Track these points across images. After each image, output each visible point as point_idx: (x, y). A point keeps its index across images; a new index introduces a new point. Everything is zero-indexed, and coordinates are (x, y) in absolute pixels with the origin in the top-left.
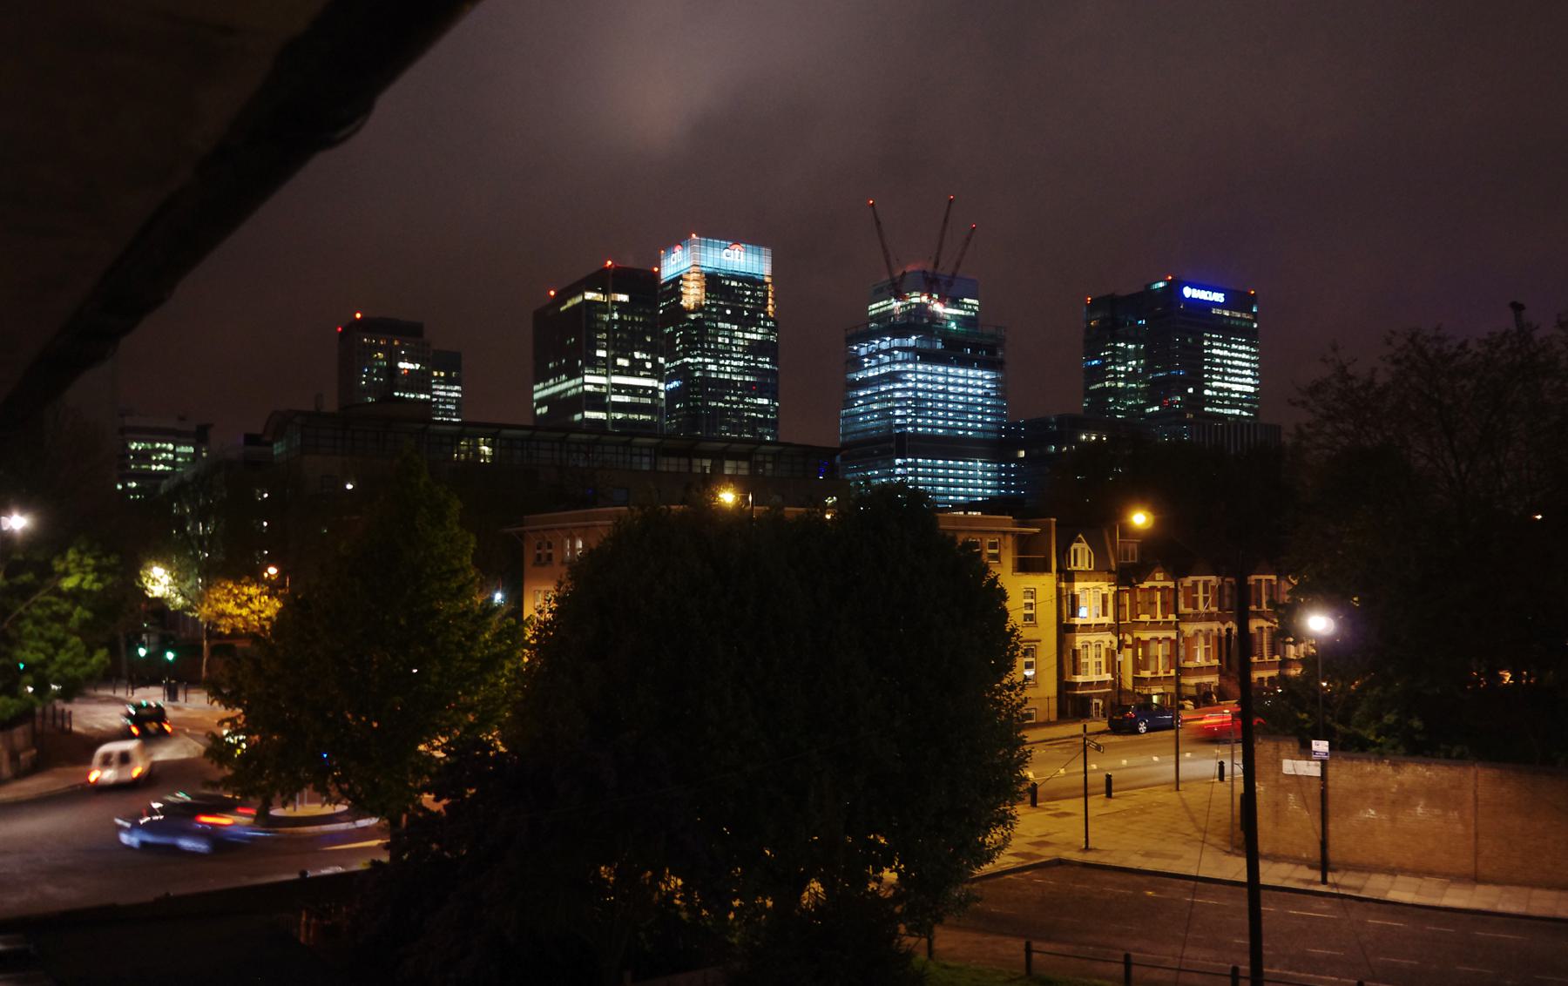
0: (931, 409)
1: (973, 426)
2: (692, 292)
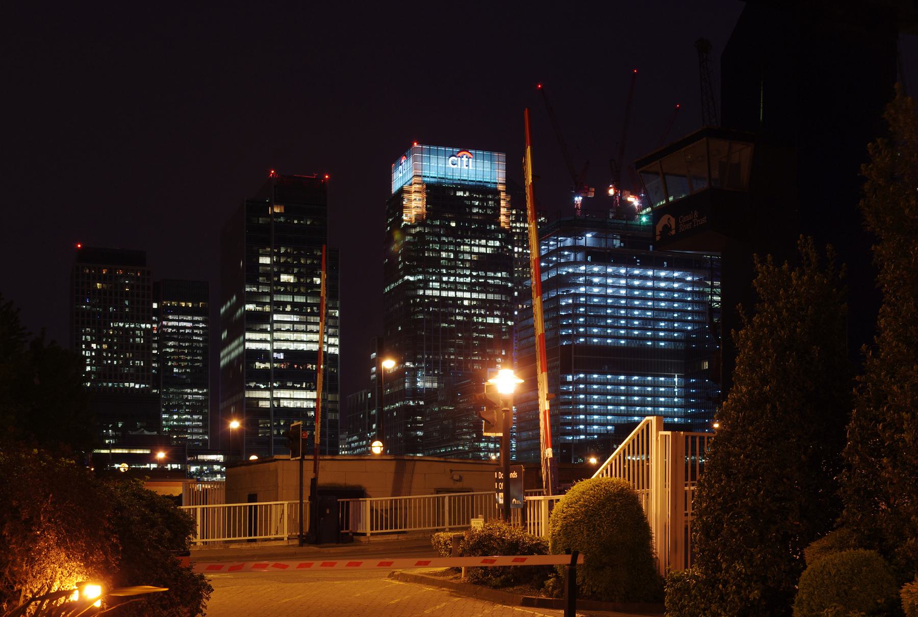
0: (611, 317)
1: (662, 337)
2: (414, 204)
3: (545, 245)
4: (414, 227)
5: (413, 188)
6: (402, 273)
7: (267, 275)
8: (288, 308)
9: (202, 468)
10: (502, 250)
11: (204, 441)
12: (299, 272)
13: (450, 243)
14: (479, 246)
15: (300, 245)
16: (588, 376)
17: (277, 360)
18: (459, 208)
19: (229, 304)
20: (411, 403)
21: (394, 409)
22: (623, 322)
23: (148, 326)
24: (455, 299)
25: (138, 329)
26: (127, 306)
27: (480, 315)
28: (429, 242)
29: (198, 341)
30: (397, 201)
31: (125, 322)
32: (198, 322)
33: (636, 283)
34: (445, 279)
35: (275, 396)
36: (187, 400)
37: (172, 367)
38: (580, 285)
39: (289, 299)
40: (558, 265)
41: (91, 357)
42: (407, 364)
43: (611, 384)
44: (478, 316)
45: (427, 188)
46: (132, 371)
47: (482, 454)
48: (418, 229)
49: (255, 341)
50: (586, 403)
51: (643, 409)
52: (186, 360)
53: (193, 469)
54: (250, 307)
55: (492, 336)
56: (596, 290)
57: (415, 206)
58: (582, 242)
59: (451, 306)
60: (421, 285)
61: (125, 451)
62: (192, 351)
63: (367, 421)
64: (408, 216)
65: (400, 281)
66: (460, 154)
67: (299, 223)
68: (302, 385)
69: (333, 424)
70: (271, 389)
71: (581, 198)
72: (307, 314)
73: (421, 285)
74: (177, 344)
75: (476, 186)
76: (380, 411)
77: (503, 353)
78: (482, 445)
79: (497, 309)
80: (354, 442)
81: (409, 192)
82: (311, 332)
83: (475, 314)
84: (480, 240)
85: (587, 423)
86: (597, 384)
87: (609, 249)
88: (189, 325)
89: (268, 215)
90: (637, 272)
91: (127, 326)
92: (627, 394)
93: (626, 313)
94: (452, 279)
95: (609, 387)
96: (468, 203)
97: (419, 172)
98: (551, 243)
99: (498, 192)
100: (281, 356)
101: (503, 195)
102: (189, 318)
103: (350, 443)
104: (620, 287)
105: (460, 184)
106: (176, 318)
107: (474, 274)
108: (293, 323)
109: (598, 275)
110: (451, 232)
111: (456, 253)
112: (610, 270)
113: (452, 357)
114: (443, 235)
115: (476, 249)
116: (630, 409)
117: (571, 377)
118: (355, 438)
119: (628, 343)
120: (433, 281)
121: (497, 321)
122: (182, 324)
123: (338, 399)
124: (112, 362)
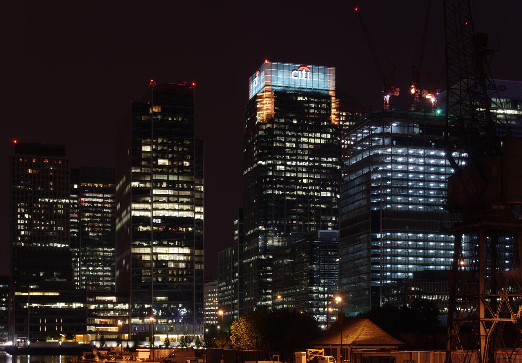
2: (265, 107)
3: (360, 133)
4: (265, 124)
6: (256, 159)
7: (148, 159)
8: (164, 185)
9: (99, 306)
10: (333, 141)
11: (112, 286)
12: (173, 157)
13: (293, 136)
14: (315, 138)
15: (174, 135)
16: (393, 235)
17: (156, 225)
18: (300, 110)
19: (121, 183)
20: (263, 257)
21: (250, 262)
23: (67, 201)
25: (60, 203)
27: (316, 190)
30: (252, 105)
31: (50, 198)
32: (107, 198)
33: (432, 161)
34: (289, 163)
35: (154, 251)
36: (99, 256)
37: (88, 231)
38: (388, 163)
39: (165, 177)
40: (370, 148)
41: (24, 224)
42: (260, 228)
44: (314, 191)
45: (275, 95)
46: (55, 234)
47: (314, 295)
48: (268, 126)
49: (139, 209)
51: (437, 259)
52: (99, 227)
53: (93, 307)
54: (135, 184)
55: (325, 206)
56: (400, 167)
57: (266, 109)
58: (389, 130)
59: (293, 183)
60: (271, 168)
61: (40, 294)
62: (103, 220)
63: (232, 270)
64: (261, 116)
65: (255, 166)
66: (300, 69)
67: (172, 120)
68: (175, 243)
69: (199, 273)
70: (151, 246)
71: (388, 96)
72: (179, 189)
73: (271, 168)
74: (91, 214)
75: (312, 92)
76: (241, 263)
77: (334, 219)
78: (314, 288)
79: (329, 186)
80: (223, 286)
81: (261, 98)
83: (312, 190)
84: (315, 133)
87: (410, 135)
89: (149, 114)
90: (432, 153)
91: (51, 201)
92: (424, 248)
93: (424, 185)
94: (294, 163)
95: (410, 243)
96: (306, 105)
97: (269, 83)
98: (366, 131)
99: (329, 97)
100: (159, 221)
101: (333, 99)
102: (101, 195)
103: (220, 288)
105: (301, 91)
106: (91, 195)
107: (311, 159)
108: (168, 196)
109: (401, 155)
111: (297, 143)
112: (411, 152)
115: (312, 141)
116: (426, 259)
117: (380, 235)
118: (224, 283)
120: (279, 165)
121: (329, 194)
123: (203, 254)
124: (41, 228)
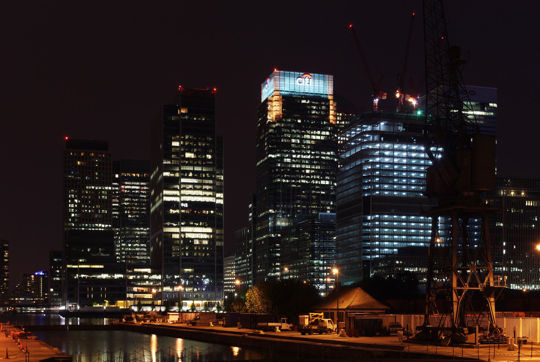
2: (274, 109)
4: (274, 123)
5: (274, 99)
7: (177, 153)
8: (191, 175)
9: (136, 277)
10: (331, 137)
11: (147, 260)
12: (197, 151)
13: (297, 133)
14: (316, 135)
15: (199, 132)
16: (381, 217)
18: (304, 111)
20: (273, 235)
22: (404, 181)
23: (110, 188)
24: (301, 169)
26: (97, 176)
27: (317, 179)
28: (284, 133)
29: (143, 198)
30: (264, 107)
31: (95, 186)
32: (143, 186)
33: (414, 155)
34: (294, 156)
35: (182, 231)
36: (137, 235)
38: (376, 156)
39: (191, 168)
40: (362, 143)
41: (74, 208)
42: (270, 211)
43: (396, 222)
44: (315, 180)
45: (282, 98)
46: (100, 216)
47: (315, 268)
48: (277, 125)
50: (379, 234)
51: (417, 238)
52: (136, 210)
53: (131, 277)
56: (387, 160)
57: (275, 110)
58: (378, 128)
59: (298, 173)
60: (279, 160)
61: (88, 266)
62: (140, 204)
64: (271, 117)
65: (266, 158)
66: (304, 76)
67: (197, 120)
68: (199, 224)
69: (220, 248)
70: (179, 227)
71: (377, 100)
72: (202, 178)
73: (279, 160)
75: (314, 96)
76: (254, 241)
77: (332, 204)
78: (315, 262)
79: (327, 175)
80: (239, 260)
81: (271, 101)
82: (205, 190)
85: (380, 247)
86: (387, 221)
87: (395, 132)
88: (138, 188)
91: (97, 188)
92: (407, 228)
94: (299, 156)
95: (395, 224)
96: (309, 107)
97: (278, 88)
100: (186, 205)
101: (331, 102)
102: (138, 183)
103: (237, 261)
104: (403, 158)
105: (304, 96)
106: (129, 183)
107: (313, 153)
109: (388, 150)
110: (298, 126)
113: (299, 206)
114: (293, 128)
115: (314, 137)
116: (409, 237)
119: (407, 194)
120: (286, 158)
121: (327, 183)
122: (133, 187)
123: (223, 233)
